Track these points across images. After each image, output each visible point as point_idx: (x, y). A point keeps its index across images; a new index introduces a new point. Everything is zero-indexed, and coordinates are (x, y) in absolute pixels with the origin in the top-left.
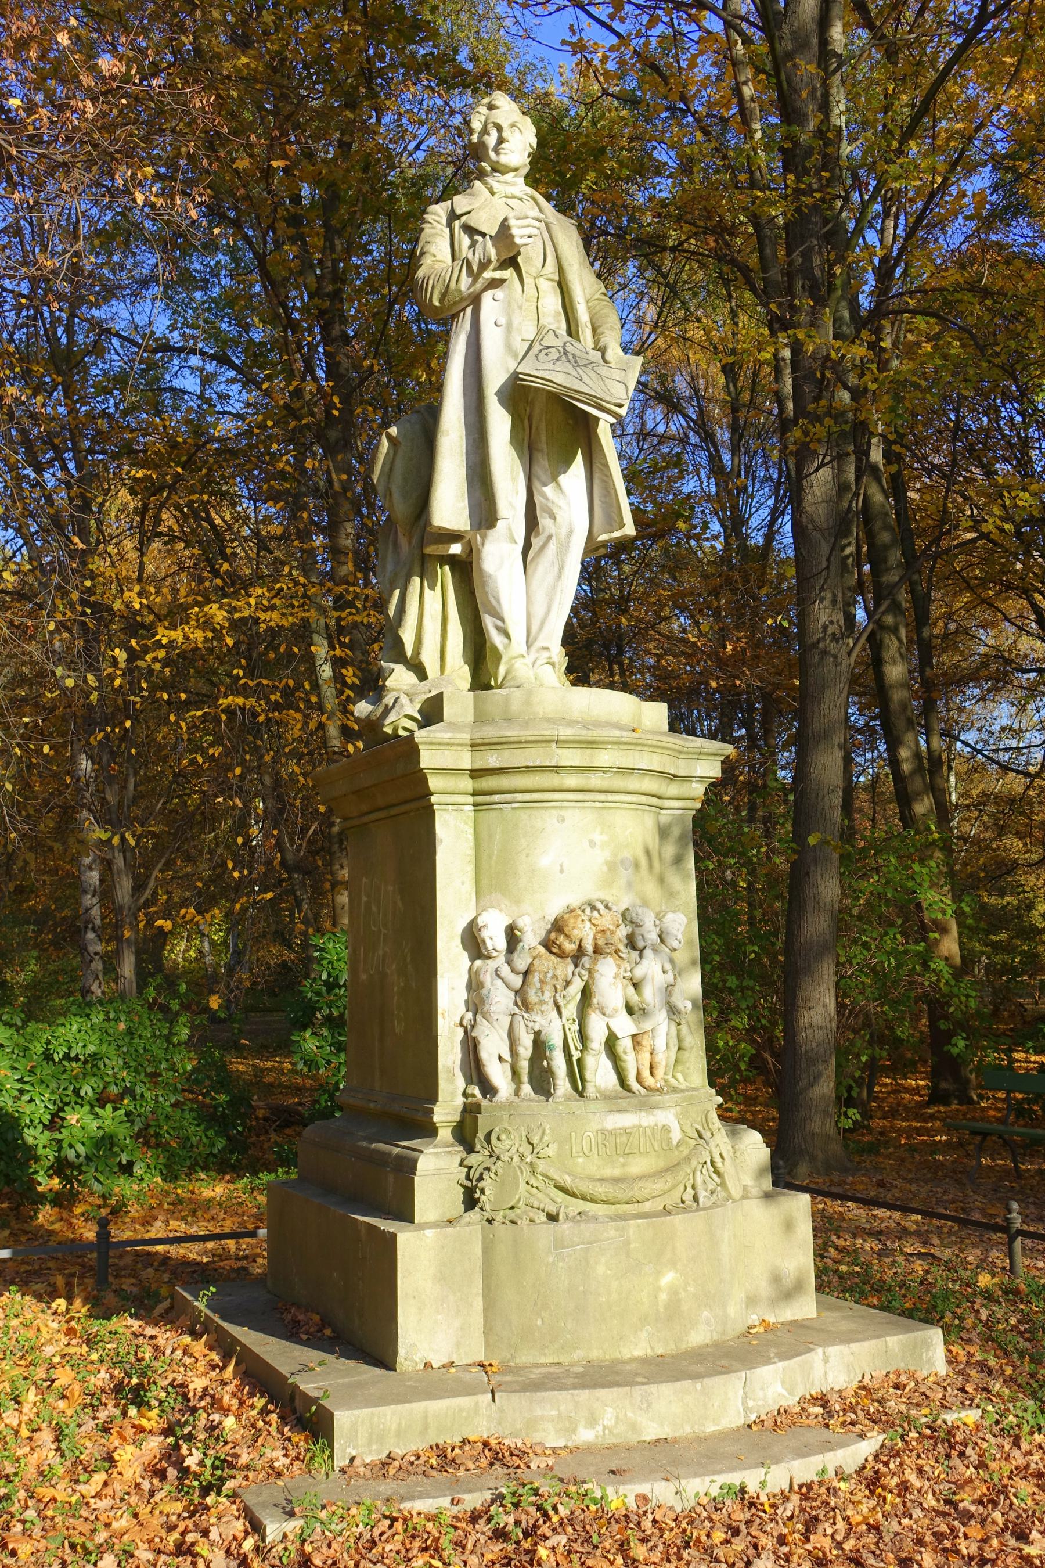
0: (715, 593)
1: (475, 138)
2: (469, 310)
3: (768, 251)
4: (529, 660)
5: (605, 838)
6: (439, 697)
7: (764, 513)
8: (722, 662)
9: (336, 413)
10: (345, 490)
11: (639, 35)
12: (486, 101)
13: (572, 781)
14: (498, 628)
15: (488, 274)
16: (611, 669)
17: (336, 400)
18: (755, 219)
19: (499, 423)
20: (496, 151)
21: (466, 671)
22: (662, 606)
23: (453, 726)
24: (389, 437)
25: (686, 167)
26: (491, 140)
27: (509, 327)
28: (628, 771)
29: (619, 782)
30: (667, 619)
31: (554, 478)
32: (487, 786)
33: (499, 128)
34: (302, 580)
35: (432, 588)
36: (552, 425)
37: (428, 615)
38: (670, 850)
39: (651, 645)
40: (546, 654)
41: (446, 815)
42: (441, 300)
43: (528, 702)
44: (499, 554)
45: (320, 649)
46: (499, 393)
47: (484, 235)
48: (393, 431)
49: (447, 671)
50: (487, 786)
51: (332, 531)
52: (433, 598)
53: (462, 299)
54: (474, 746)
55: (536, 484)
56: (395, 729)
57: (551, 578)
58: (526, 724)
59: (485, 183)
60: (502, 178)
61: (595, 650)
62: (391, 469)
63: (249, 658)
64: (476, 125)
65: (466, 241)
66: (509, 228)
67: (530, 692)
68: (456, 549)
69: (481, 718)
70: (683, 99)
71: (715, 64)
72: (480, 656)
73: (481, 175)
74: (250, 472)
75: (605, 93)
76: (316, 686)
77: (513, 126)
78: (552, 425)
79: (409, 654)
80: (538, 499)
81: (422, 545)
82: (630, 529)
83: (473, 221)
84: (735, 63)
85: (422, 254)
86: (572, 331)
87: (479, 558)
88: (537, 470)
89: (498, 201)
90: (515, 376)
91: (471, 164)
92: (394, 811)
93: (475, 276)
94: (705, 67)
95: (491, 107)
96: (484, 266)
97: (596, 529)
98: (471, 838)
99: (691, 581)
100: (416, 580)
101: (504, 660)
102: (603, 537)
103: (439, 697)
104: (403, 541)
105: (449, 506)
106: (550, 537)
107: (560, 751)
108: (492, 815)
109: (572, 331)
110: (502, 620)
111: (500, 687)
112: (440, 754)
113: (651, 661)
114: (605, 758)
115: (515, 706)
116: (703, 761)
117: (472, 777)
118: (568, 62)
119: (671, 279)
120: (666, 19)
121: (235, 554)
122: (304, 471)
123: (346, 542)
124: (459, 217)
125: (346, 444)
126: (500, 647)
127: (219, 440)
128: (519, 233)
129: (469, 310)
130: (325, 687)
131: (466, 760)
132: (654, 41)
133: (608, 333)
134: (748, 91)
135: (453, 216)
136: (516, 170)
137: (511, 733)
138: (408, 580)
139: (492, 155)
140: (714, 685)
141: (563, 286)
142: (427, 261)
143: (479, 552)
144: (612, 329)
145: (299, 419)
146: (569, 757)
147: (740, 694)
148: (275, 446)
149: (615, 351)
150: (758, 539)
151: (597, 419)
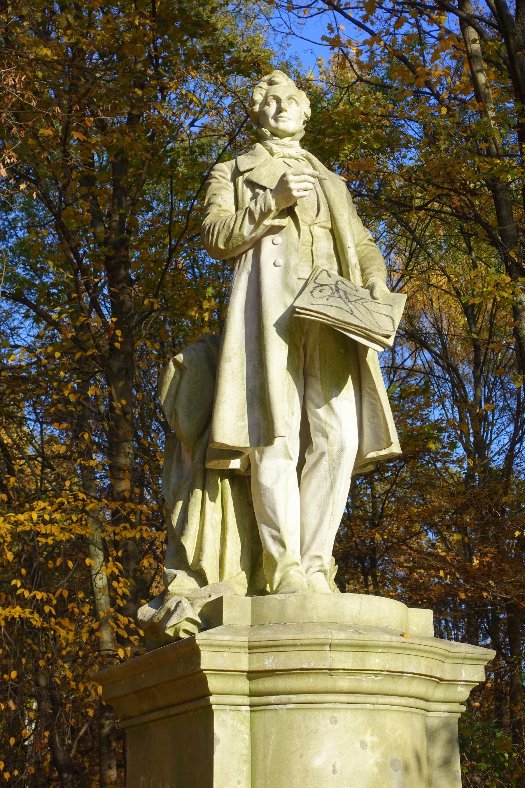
0: (461, 510)
1: (257, 108)
2: (251, 253)
3: (504, 213)
4: (302, 568)
5: (376, 739)
6: (219, 602)
7: (505, 439)
8: (469, 576)
9: (117, 345)
10: (125, 413)
11: (388, 33)
12: (266, 78)
13: (344, 683)
14: (274, 538)
15: (268, 222)
16: (366, 579)
17: (118, 333)
18: (493, 183)
19: (277, 351)
20: (276, 118)
21: (243, 578)
22: (412, 522)
23: (233, 630)
24: (176, 363)
25: (431, 138)
26: (271, 110)
27: (287, 269)
28: (397, 674)
29: (389, 685)
30: (418, 534)
31: (327, 401)
32: (263, 687)
33: (278, 100)
34: (81, 496)
35: (213, 499)
36: (326, 353)
37: (209, 525)
38: (438, 752)
39: (402, 559)
40: (318, 563)
41: (224, 716)
42: (226, 244)
43: (302, 607)
44: (276, 470)
45: (96, 561)
46: (277, 325)
47: (264, 189)
48: (180, 357)
49: (226, 577)
50: (263, 687)
51: (112, 450)
52: (213, 509)
53: (245, 243)
54: (252, 648)
55: (310, 406)
56: (177, 632)
57: (323, 492)
58: (301, 628)
59: (265, 146)
60: (280, 141)
61: (358, 563)
62: (177, 392)
63: (29, 568)
64: (258, 97)
65: (248, 194)
66: (287, 182)
67: (304, 598)
68: (235, 464)
69: (258, 622)
70: (428, 84)
71: (453, 57)
72: (257, 564)
73: (261, 138)
74: (38, 396)
75: (360, 79)
76: (90, 592)
77: (290, 98)
78: (326, 353)
79: (190, 561)
80: (312, 419)
81: (204, 461)
82: (396, 448)
83: (254, 177)
84: (471, 57)
85: (209, 204)
86: (343, 270)
87: (257, 472)
88: (312, 394)
89: (277, 160)
90: (292, 310)
91: (252, 128)
92: (173, 711)
93: (256, 223)
94: (447, 61)
95: (271, 83)
96: (264, 215)
97: (365, 447)
98: (247, 737)
99: (435, 500)
100: (198, 492)
101: (279, 567)
102: (372, 455)
103: (219, 602)
104: (186, 457)
105: (231, 425)
106: (323, 454)
107: (333, 654)
108: (268, 715)
109: (343, 270)
110: (278, 530)
111: (276, 592)
112: (220, 656)
113: (402, 574)
114: (375, 661)
115: (291, 611)
116: (468, 665)
117: (249, 678)
118: (327, 55)
119: (418, 232)
120: (413, 21)
121: (22, 471)
122: (87, 398)
123: (123, 461)
124: (242, 173)
125: (128, 372)
126: (276, 555)
127: (12, 368)
128: (296, 187)
129: (251, 253)
130: (99, 596)
131: (243, 662)
132: (399, 38)
133: (375, 273)
134: (482, 78)
135: (237, 173)
136: (293, 135)
137: (287, 636)
138: (190, 492)
139: (272, 122)
140: (463, 596)
141: (334, 232)
142: (213, 211)
143: (257, 467)
144: (379, 270)
145: (85, 350)
146: (342, 660)
147: (486, 605)
148: (62, 374)
149: (382, 288)
150: (498, 462)
151: (366, 348)
